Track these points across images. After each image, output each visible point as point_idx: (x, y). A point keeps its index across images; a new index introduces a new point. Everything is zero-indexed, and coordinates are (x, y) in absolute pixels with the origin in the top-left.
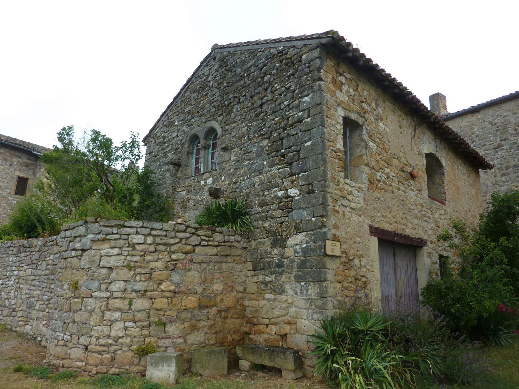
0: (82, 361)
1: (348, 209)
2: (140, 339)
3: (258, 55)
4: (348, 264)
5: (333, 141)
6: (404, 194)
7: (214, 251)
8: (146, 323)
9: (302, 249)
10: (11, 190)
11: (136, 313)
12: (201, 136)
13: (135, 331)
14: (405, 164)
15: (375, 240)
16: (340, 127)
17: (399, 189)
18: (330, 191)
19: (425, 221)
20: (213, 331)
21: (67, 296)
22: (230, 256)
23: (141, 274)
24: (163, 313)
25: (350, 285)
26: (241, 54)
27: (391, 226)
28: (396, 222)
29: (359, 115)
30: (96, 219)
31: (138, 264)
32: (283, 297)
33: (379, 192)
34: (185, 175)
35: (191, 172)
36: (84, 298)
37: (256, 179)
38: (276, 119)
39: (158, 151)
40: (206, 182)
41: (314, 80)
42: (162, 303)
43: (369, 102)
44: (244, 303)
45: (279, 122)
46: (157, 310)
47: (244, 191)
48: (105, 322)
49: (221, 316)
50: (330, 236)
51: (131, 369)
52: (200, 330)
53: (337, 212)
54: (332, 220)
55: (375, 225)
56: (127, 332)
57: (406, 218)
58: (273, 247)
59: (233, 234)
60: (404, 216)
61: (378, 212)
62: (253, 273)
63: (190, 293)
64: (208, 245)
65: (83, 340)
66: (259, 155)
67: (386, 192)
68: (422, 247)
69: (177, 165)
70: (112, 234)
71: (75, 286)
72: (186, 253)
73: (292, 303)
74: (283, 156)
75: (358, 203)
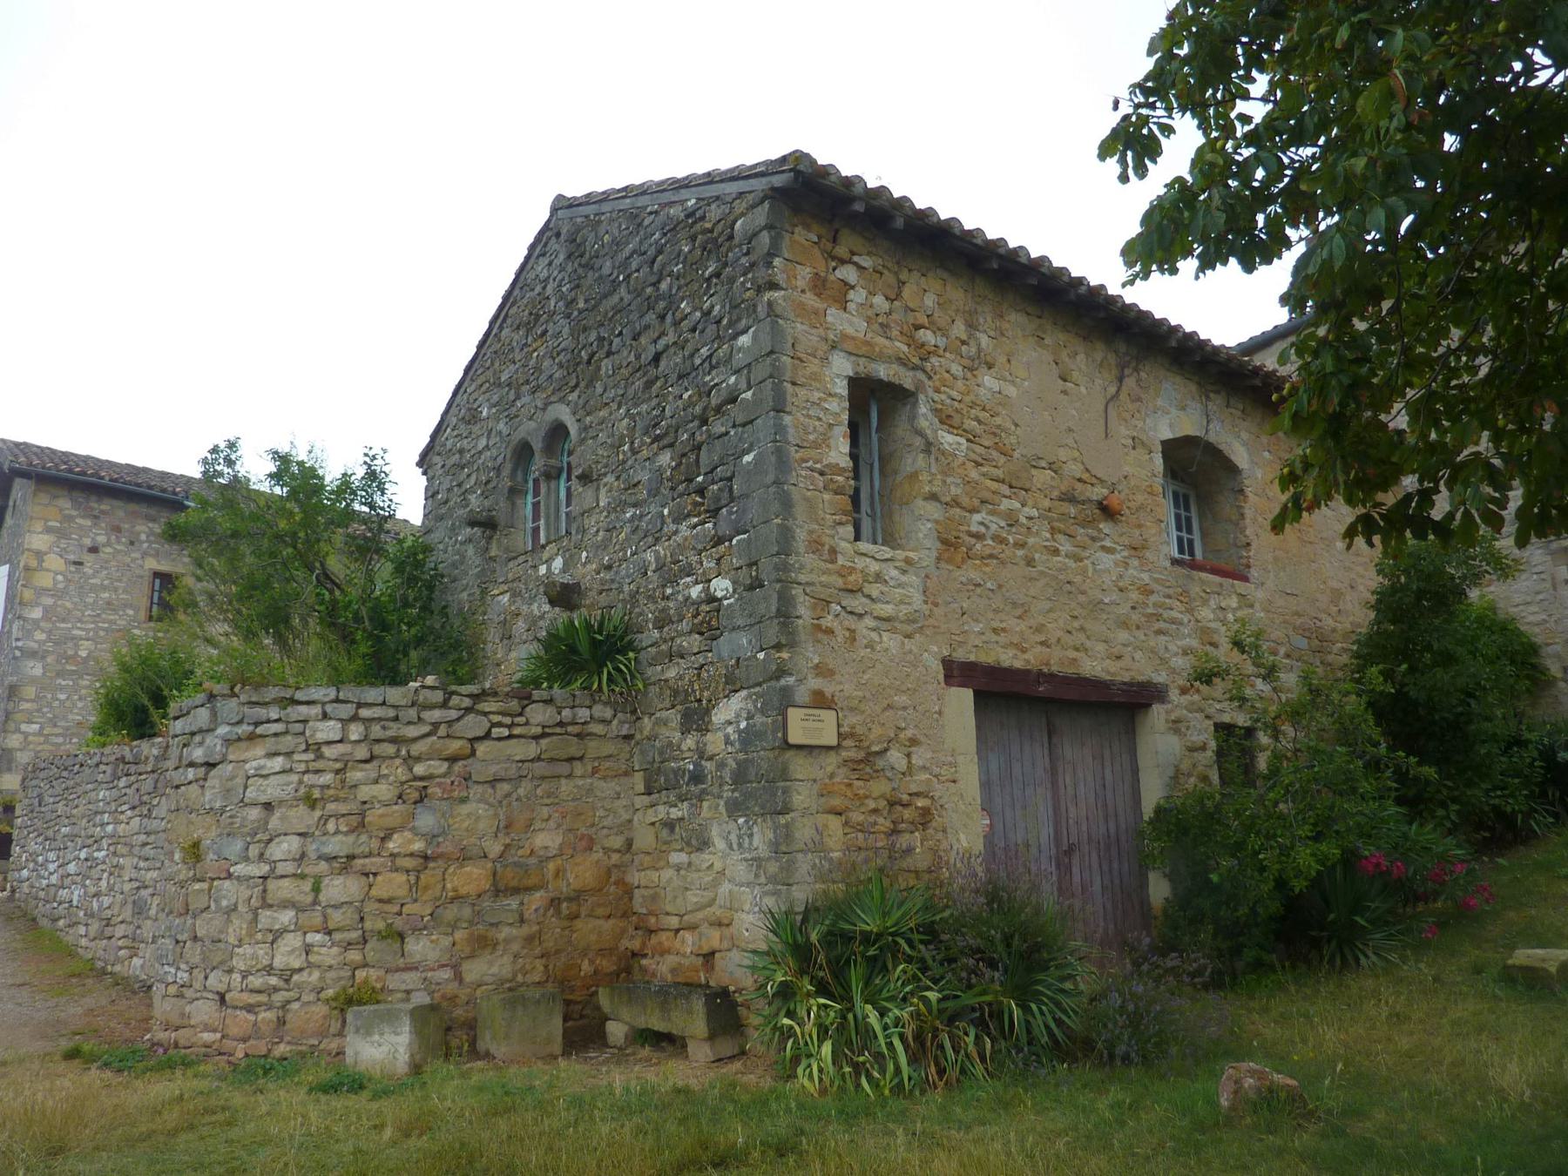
0: (215, 1031)
1: (869, 621)
2: (342, 974)
3: (646, 222)
4: (866, 763)
5: (816, 445)
7: (532, 749)
8: (355, 935)
9: (740, 732)
10: (137, 610)
11: (329, 911)
12: (537, 445)
13: (328, 954)
14: (1080, 480)
15: (964, 698)
16: (839, 408)
17: (1056, 552)
18: (802, 578)
19: (1160, 632)
20: (538, 951)
21: (182, 877)
22: (581, 758)
23: (338, 816)
24: (396, 909)
25: (872, 819)
26: (612, 220)
27: (1026, 656)
28: (1042, 643)
29: (905, 365)
30: (232, 689)
31: (331, 792)
32: (705, 858)
34: (507, 550)
35: (523, 541)
37: (649, 556)
38: (686, 396)
39: (449, 490)
40: (549, 569)
41: (759, 290)
42: (392, 884)
43: (942, 322)
44: (628, 879)
45: (690, 404)
47: (626, 588)
48: (259, 936)
49: (558, 912)
50: (802, 695)
51: (322, 1046)
52: (501, 947)
53: (830, 632)
54: (811, 654)
55: (961, 655)
56: (313, 958)
57: (1082, 629)
58: (685, 731)
59: (588, 703)
60: (1076, 624)
61: (977, 620)
62: (646, 799)
63: (464, 857)
65: (216, 981)
66: (654, 493)
69: (488, 524)
70: (268, 721)
71: (194, 852)
72: (452, 759)
73: (722, 873)
74: (701, 491)
75: (902, 602)
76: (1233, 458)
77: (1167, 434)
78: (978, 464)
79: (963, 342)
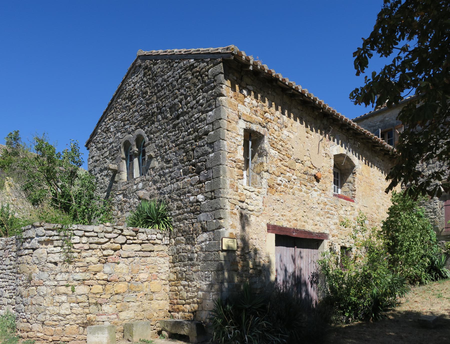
3: (175, 65)
6: (306, 195)
7: (139, 247)
8: (86, 304)
11: (78, 296)
14: (310, 167)
16: (241, 139)
17: (301, 191)
18: (228, 197)
27: (290, 224)
28: (295, 220)
29: (261, 126)
33: (278, 195)
36: (37, 286)
42: (97, 288)
46: (94, 294)
55: (272, 223)
56: (72, 311)
61: (277, 212)
64: (133, 243)
67: (286, 194)
68: (323, 240)
72: (115, 250)
76: (354, 161)
77: (336, 153)
78: (281, 161)
79: (279, 118)
